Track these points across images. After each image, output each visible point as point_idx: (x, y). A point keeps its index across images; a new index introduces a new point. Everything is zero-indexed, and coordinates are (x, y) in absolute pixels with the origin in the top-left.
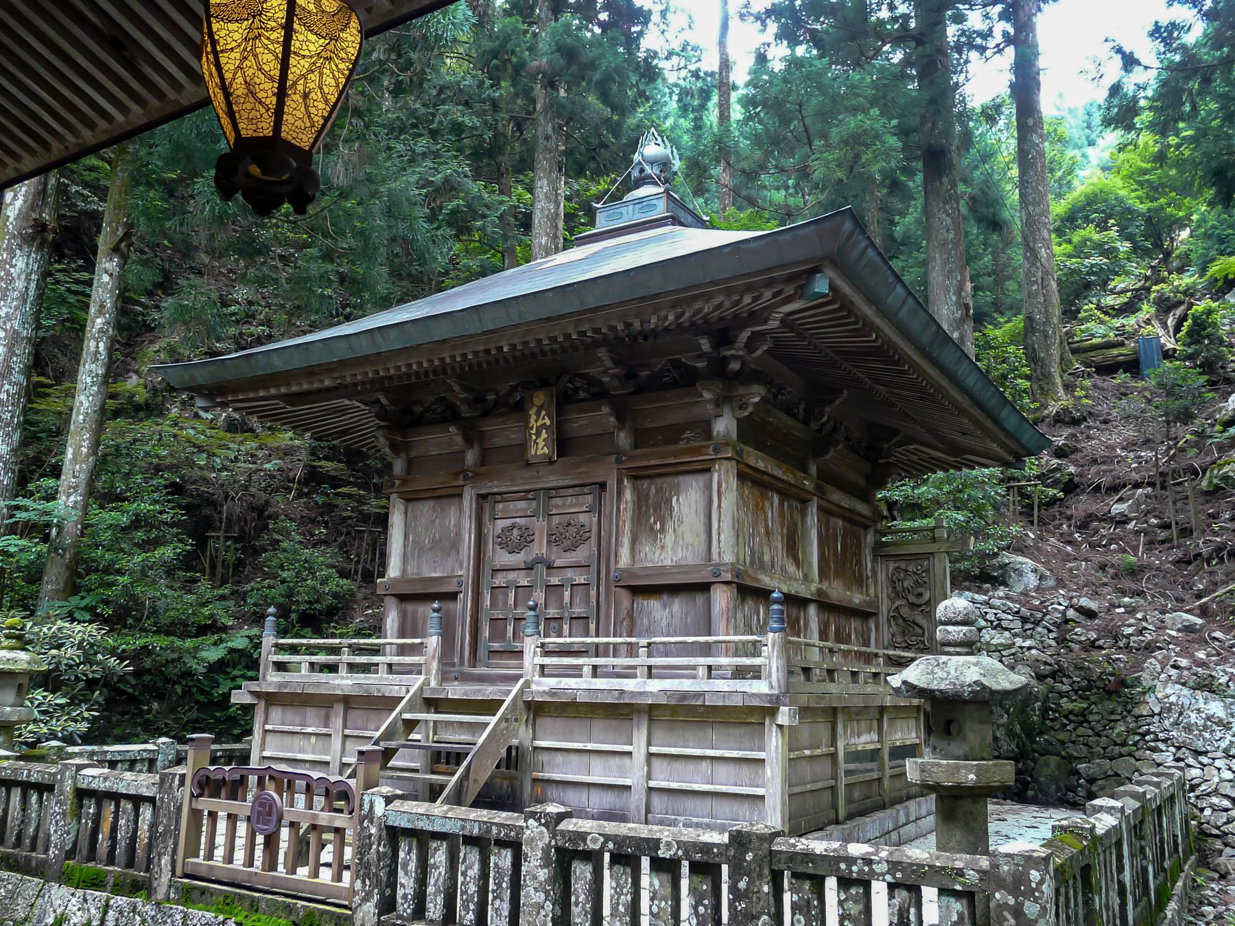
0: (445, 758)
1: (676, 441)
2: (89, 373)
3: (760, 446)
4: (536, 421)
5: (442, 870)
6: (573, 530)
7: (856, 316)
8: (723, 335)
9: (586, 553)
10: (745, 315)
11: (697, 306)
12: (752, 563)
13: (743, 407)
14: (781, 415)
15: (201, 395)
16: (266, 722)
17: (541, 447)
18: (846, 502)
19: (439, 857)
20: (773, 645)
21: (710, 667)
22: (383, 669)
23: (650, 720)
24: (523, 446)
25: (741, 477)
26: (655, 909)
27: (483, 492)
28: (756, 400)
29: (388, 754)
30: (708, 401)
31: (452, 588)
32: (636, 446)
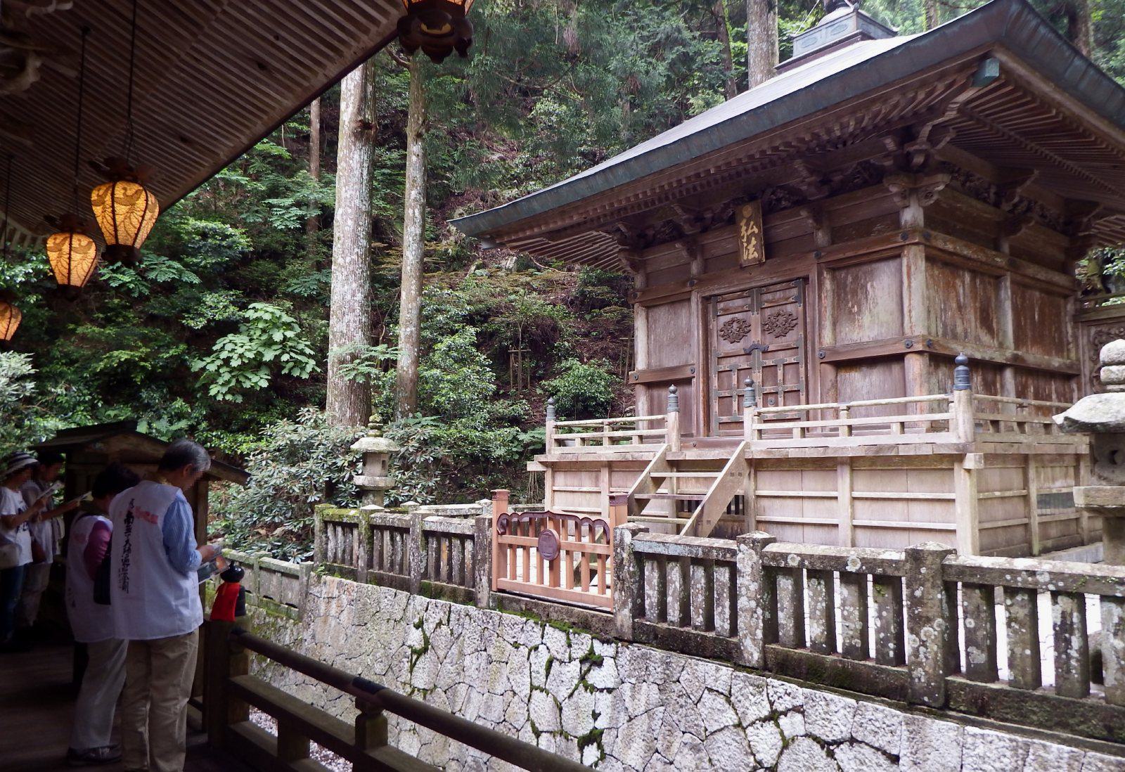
0: (685, 506)
1: (869, 233)
2: (411, 232)
3: (949, 231)
4: (747, 230)
5: (678, 585)
6: (781, 319)
7: (1032, 94)
8: (907, 134)
9: (795, 337)
10: (924, 110)
11: (875, 108)
12: (945, 334)
13: (928, 195)
14: (974, 202)
15: (486, 240)
16: (553, 485)
17: (751, 252)
18: (1043, 274)
19: (675, 574)
20: (959, 401)
21: (902, 424)
22: (635, 439)
23: (852, 470)
24: (737, 253)
25: (930, 259)
26: (846, 613)
27: (707, 294)
28: (941, 187)
29: (642, 503)
30: (896, 194)
31: (688, 374)
32: (833, 242)
